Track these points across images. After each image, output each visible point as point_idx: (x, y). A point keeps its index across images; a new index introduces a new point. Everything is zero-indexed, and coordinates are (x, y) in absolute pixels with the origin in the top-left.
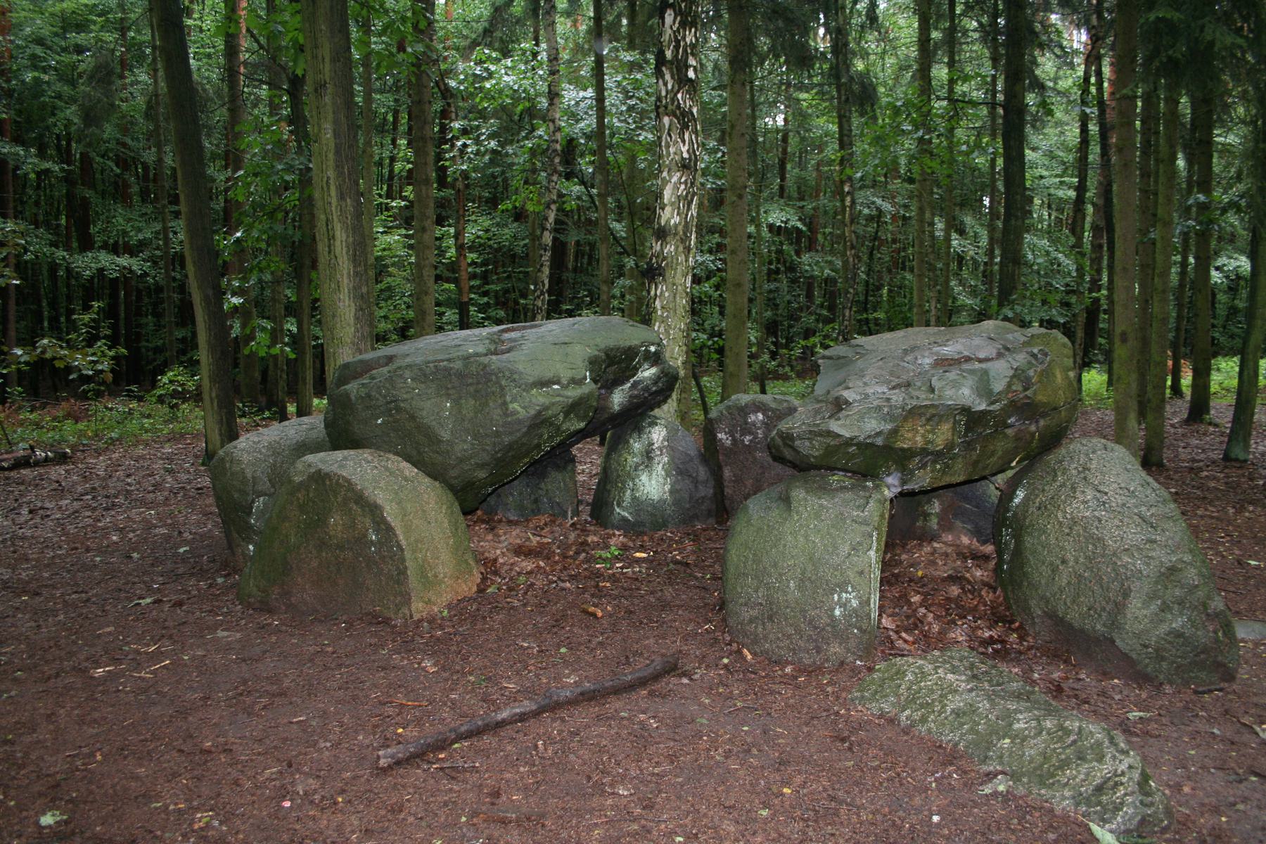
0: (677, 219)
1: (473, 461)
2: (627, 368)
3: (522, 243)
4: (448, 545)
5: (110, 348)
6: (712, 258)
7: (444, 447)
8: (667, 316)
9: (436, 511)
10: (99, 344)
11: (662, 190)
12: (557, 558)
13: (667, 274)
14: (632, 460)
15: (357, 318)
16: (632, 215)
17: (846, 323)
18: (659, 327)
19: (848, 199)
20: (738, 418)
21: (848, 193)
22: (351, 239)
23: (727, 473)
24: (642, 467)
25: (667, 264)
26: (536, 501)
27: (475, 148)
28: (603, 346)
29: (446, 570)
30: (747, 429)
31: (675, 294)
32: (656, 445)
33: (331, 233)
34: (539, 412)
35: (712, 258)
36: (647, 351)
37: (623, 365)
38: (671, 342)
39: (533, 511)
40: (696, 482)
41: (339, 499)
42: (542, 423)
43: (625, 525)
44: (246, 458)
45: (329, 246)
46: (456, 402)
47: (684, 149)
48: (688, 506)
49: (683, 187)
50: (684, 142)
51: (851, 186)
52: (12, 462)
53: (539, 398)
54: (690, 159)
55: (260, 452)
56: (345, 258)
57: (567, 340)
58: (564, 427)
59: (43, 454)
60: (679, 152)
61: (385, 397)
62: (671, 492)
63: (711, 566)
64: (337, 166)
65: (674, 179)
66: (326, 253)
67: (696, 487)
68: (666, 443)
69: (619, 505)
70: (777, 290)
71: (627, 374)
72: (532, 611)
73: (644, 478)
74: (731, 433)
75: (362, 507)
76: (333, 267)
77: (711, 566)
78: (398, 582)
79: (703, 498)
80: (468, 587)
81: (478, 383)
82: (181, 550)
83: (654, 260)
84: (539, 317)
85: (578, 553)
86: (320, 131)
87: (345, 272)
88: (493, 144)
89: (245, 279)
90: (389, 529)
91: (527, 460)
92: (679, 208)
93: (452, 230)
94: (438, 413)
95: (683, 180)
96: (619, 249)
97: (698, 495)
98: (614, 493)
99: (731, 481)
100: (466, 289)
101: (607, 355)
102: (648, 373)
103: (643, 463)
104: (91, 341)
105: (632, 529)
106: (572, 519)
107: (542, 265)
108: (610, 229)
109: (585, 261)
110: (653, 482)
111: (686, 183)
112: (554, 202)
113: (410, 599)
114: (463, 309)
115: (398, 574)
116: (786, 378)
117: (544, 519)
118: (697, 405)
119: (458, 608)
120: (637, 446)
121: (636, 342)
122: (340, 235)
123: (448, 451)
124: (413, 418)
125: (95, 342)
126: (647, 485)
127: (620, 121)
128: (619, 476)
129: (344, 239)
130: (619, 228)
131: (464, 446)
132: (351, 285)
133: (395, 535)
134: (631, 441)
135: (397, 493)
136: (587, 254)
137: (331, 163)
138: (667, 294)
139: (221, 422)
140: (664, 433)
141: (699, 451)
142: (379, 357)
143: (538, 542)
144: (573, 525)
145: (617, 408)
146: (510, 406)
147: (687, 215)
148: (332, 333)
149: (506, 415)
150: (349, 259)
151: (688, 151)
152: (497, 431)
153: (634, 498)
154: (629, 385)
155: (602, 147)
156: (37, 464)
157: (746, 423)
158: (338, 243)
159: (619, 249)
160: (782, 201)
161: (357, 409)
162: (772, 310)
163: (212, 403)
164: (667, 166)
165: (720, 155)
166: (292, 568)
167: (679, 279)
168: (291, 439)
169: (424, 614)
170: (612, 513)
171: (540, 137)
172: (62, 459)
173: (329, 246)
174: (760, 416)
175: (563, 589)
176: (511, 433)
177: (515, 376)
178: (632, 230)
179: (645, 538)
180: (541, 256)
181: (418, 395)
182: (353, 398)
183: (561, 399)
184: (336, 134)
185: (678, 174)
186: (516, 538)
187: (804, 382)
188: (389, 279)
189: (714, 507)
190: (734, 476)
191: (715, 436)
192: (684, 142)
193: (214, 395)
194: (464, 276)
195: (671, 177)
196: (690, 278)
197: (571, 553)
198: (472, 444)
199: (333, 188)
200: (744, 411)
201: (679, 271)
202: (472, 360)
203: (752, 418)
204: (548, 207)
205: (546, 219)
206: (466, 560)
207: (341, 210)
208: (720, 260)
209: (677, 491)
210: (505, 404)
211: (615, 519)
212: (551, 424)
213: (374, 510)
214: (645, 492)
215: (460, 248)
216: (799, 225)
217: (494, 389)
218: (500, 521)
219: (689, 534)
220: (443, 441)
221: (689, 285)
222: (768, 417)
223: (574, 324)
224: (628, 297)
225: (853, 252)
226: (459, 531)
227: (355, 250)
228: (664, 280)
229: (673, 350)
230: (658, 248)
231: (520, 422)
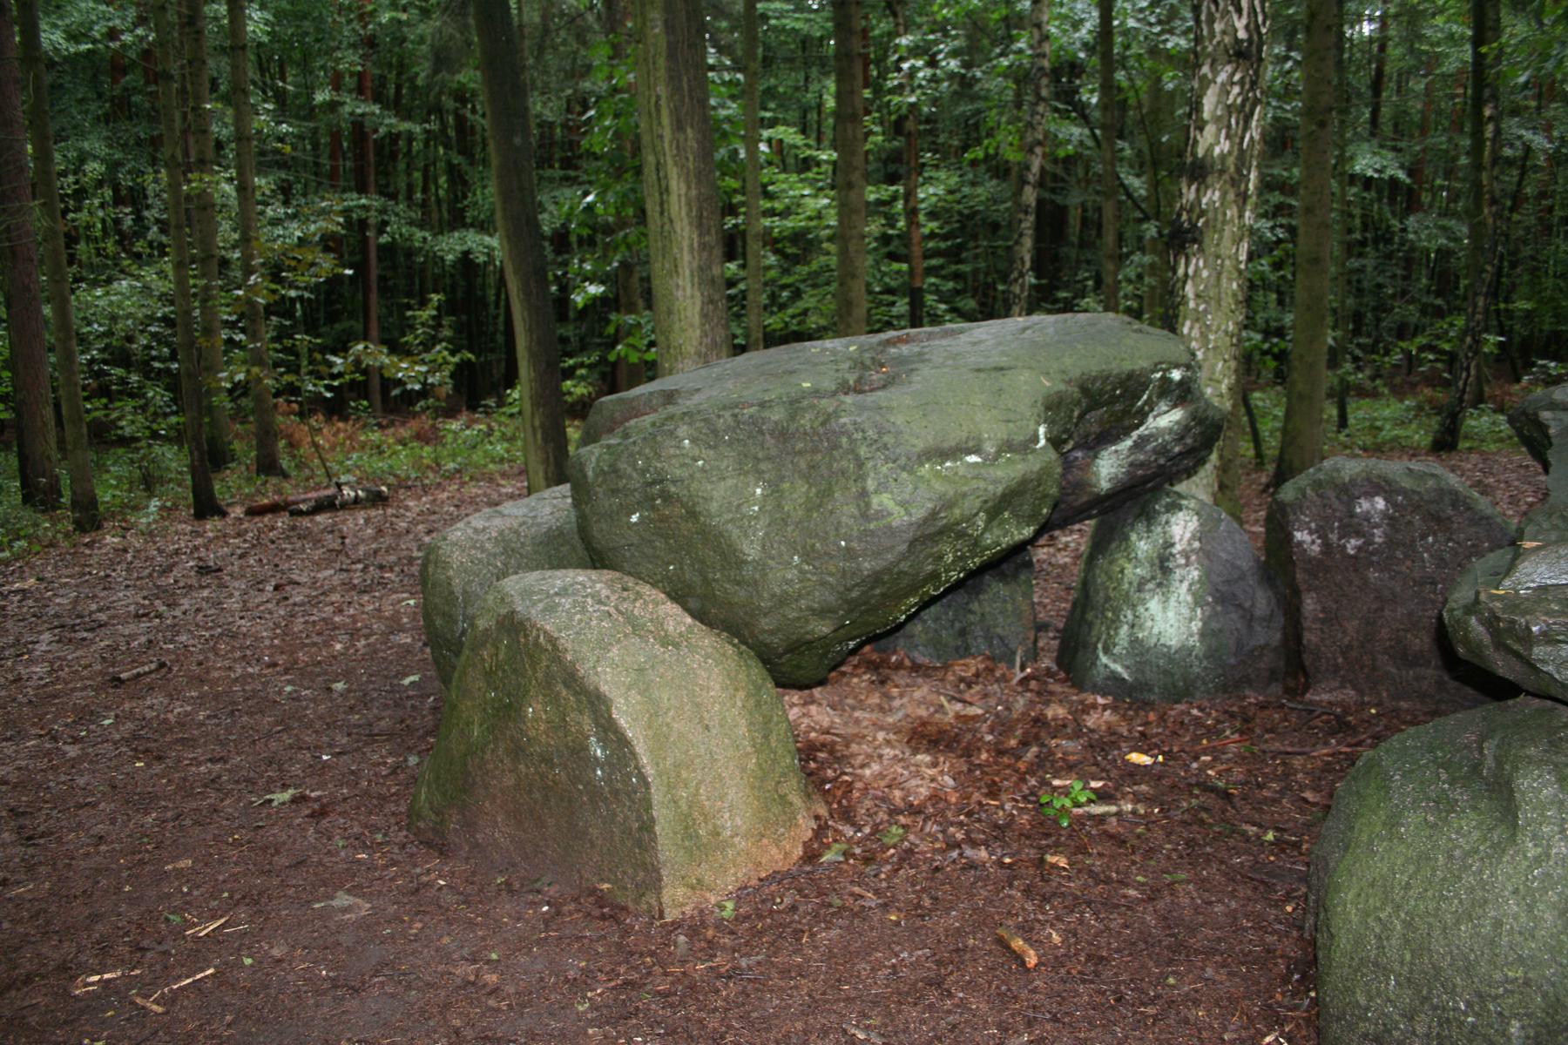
0: (1224, 146)
1: (803, 603)
2: (1126, 413)
3: (1002, 207)
4: (743, 770)
5: (453, 353)
6: (1270, 224)
7: (748, 572)
8: (1205, 311)
9: (723, 704)
10: (438, 347)
11: (1201, 96)
12: (984, 756)
13: (1207, 240)
14: (1134, 572)
15: (705, 316)
16: (1156, 164)
17: (1478, 317)
18: (1191, 328)
19: (1490, 128)
20: (1336, 504)
21: (1490, 118)
22: (694, 193)
23: (1310, 604)
24: (1150, 586)
25: (1206, 223)
26: (963, 633)
27: (928, 72)
28: (1075, 373)
29: (739, 821)
30: (1353, 526)
31: (1219, 274)
32: (1178, 548)
33: (663, 183)
34: (934, 515)
35: (1270, 224)
36: (1166, 380)
37: (1118, 407)
38: (1211, 354)
39: (957, 649)
40: (1249, 618)
41: (540, 675)
42: (941, 532)
43: (1114, 686)
44: (456, 557)
45: (662, 204)
46: (774, 489)
47: (1240, 24)
48: (1232, 661)
49: (1236, 90)
50: (1239, 11)
51: (1496, 107)
52: (312, 503)
53: (935, 481)
54: (1250, 40)
55: (483, 549)
56: (686, 221)
57: (1003, 361)
58: (988, 539)
59: (352, 494)
60: (1230, 29)
61: (643, 472)
62: (1203, 634)
63: (1274, 801)
64: (671, 78)
65: (1222, 77)
66: (657, 215)
67: (1250, 627)
68: (1196, 545)
69: (1107, 651)
70: (1362, 270)
71: (1126, 423)
72: (897, 924)
73: (1154, 605)
74: (1321, 532)
75: (576, 694)
76: (667, 236)
77: (1274, 801)
78: (639, 843)
79: (1263, 647)
80: (784, 852)
81: (815, 451)
82: (407, 681)
83: (1184, 217)
84: (1016, 309)
85: (1025, 744)
86: (644, 24)
87: (685, 244)
88: (953, 64)
89: (605, 258)
90: (623, 742)
91: (913, 600)
92: (1229, 127)
93: (901, 189)
94: (739, 506)
95: (1237, 78)
96: (1138, 215)
97: (1253, 643)
98: (1099, 628)
99: (1316, 620)
100: (919, 270)
101: (1084, 390)
102: (1166, 419)
103: (1153, 578)
104: (427, 346)
105: (1129, 695)
106: (1023, 668)
107: (1021, 235)
108: (1122, 185)
109: (1094, 232)
110: (1171, 614)
111: (1242, 82)
112: (1040, 143)
113: (660, 880)
114: (916, 297)
115: (640, 829)
116: (1374, 394)
117: (974, 665)
118: (1244, 433)
119: (756, 898)
120: (1143, 546)
121: (1142, 363)
122: (677, 185)
123: (756, 582)
124: (693, 514)
125: (434, 345)
126: (1158, 618)
127: (1139, 20)
128: (1108, 599)
129: (683, 191)
130: (1137, 184)
131: (788, 573)
132: (695, 265)
133: (634, 754)
134: (1134, 537)
135: (641, 670)
136: (1093, 224)
137: (662, 73)
138: (1205, 274)
139: (546, 461)
140: (1194, 524)
141: (1257, 560)
142: (651, 394)
143: (958, 716)
144: (1024, 681)
145: (1105, 485)
146: (875, 500)
147: (1242, 138)
148: (667, 339)
149: (865, 516)
150: (691, 224)
151: (1247, 27)
152: (847, 549)
153: (1135, 642)
154: (1129, 443)
155: (1109, 63)
156: (345, 506)
157: (1352, 515)
158: (674, 198)
159: (1138, 215)
160: (1375, 142)
161: (596, 493)
162: (1356, 297)
163: (535, 435)
164: (1209, 55)
165: (1289, 65)
166: (475, 783)
167: (1227, 248)
168: (539, 525)
169: (688, 910)
170: (1094, 664)
171: (1020, 51)
172: (377, 499)
173: (662, 204)
174: (1380, 503)
175: (972, 865)
176: (877, 554)
177: (886, 439)
178: (1155, 185)
179: (1152, 716)
180: (1021, 221)
181: (703, 470)
182: (590, 474)
183: (982, 485)
184: (669, 27)
185: (1229, 68)
186: (919, 703)
187: (1401, 401)
188: (823, 259)
189: (1282, 663)
190: (1324, 610)
191: (1290, 536)
192: (1239, 11)
193: (537, 423)
194: (917, 251)
195: (1216, 73)
196: (1245, 246)
197: (1013, 743)
198: (802, 572)
199: (665, 113)
200: (1348, 492)
201: (1227, 233)
202: (805, 403)
203: (1363, 506)
204: (1031, 151)
205: (1028, 168)
206: (782, 797)
207: (678, 147)
208: (1281, 226)
209: (1214, 633)
210: (864, 494)
211: (1099, 675)
212: (961, 535)
213: (596, 703)
214: (1155, 631)
215: (911, 213)
216: (1401, 175)
217: (844, 463)
218: (899, 666)
219: (1232, 716)
220: (746, 562)
221: (1243, 257)
222: (1395, 505)
223: (1025, 329)
224: (1147, 280)
225: (1494, 209)
226: (773, 738)
227: (700, 209)
228: (1201, 250)
229: (1213, 367)
230: (1192, 196)
231: (891, 531)
